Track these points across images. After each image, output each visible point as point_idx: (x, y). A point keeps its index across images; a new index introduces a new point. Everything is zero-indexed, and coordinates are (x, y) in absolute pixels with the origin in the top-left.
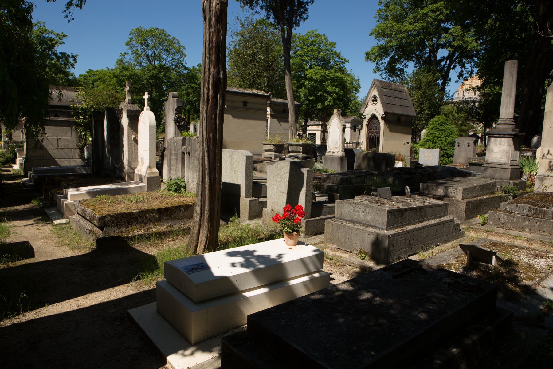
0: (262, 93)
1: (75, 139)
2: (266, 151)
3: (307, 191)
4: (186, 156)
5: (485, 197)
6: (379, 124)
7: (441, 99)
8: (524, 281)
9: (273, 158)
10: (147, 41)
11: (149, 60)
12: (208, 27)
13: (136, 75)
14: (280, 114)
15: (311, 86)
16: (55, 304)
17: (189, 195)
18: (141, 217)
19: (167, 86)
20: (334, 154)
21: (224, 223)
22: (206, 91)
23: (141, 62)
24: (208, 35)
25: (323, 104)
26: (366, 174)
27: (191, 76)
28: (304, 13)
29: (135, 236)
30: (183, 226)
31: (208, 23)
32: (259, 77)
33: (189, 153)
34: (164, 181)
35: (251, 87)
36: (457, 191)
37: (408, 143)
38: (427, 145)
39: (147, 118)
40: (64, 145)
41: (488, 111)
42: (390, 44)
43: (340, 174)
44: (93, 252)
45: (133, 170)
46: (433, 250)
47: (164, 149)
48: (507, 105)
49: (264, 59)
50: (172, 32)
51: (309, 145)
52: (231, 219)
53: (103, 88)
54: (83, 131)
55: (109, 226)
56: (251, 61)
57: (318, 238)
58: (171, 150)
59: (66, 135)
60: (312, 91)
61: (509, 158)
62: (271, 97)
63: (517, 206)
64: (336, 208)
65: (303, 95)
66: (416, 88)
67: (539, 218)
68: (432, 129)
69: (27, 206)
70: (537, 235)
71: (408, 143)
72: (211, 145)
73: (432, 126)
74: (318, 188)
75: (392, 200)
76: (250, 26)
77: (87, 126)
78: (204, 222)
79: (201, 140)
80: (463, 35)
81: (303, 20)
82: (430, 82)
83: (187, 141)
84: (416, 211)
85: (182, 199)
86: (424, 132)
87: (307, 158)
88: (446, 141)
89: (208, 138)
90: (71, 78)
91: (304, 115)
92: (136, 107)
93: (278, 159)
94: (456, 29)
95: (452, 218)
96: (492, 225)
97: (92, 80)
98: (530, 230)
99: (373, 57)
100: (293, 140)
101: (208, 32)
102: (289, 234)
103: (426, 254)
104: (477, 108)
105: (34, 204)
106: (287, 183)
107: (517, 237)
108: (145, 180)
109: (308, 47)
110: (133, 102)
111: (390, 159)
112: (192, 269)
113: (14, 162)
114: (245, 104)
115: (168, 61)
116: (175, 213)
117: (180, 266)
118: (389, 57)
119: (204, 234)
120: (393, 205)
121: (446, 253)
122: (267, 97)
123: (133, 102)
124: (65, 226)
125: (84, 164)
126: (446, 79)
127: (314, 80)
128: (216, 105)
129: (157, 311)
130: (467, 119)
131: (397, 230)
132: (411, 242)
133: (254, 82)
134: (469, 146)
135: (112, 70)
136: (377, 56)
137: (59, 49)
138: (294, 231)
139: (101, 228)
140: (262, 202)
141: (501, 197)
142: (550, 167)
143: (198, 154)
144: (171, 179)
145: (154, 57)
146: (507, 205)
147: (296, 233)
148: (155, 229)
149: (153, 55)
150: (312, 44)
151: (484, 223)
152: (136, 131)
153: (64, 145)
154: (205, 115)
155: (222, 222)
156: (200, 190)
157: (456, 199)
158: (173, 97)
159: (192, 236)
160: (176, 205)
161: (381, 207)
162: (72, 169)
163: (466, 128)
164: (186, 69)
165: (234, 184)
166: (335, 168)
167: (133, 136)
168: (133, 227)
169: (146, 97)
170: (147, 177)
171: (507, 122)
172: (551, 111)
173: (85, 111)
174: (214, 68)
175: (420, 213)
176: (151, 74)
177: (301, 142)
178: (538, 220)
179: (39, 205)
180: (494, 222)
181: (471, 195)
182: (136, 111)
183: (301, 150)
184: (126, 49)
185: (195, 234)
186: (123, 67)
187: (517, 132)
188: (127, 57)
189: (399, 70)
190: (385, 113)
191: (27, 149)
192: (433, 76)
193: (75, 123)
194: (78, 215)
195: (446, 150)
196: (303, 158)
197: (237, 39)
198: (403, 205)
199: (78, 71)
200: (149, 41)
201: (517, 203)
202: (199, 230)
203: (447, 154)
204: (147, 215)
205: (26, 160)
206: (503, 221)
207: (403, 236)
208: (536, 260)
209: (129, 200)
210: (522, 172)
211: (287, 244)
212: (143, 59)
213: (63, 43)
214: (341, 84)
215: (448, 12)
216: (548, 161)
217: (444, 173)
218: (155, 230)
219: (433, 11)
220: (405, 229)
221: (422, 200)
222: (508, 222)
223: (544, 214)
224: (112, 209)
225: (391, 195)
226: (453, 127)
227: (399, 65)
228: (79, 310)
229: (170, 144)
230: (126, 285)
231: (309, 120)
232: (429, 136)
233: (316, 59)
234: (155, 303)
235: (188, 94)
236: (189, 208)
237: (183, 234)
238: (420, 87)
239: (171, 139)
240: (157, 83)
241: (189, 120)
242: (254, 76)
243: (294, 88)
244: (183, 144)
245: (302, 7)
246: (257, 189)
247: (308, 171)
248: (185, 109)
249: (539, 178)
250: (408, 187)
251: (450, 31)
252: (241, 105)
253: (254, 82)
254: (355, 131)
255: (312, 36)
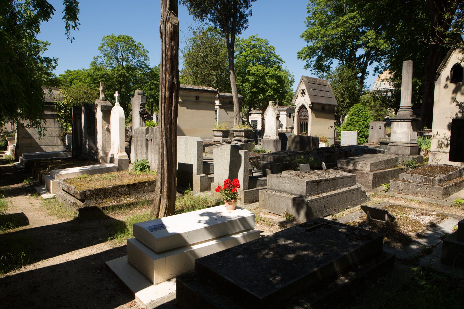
0: (211, 89)
1: (57, 129)
2: (215, 136)
3: (245, 168)
4: (149, 142)
5: (389, 170)
6: (307, 112)
7: (360, 90)
8: (410, 233)
9: (221, 142)
10: (117, 46)
11: (118, 62)
12: (164, 44)
13: (107, 74)
14: (227, 105)
15: (254, 81)
16: (49, 259)
17: (152, 173)
18: (114, 191)
19: (133, 83)
20: (270, 138)
21: (180, 195)
22: (163, 93)
23: (112, 63)
24: (164, 50)
25: (264, 94)
26: (297, 152)
27: (153, 75)
28: (245, 22)
29: (110, 206)
30: (147, 198)
31: (164, 41)
32: (209, 76)
33: (152, 140)
34: (132, 162)
35: (202, 84)
36: (365, 165)
37: (332, 127)
38: (348, 129)
39: (117, 112)
40: (51, 137)
41: (394, 101)
42: (317, 45)
43: (273, 154)
44: (76, 219)
45: (106, 154)
46: (344, 212)
47: (132, 137)
48: (405, 96)
49: (213, 60)
50: (137, 40)
51: (250, 131)
52: (186, 192)
53: (80, 86)
54: (64, 123)
55: (88, 199)
56: (202, 62)
57: (255, 205)
58: (137, 137)
59: (50, 127)
60: (255, 85)
61: (408, 138)
62: (219, 92)
63: (412, 176)
64: (267, 181)
65: (247, 88)
66: (339, 82)
67: (429, 185)
68: (352, 115)
69: (20, 185)
70: (427, 199)
71: (332, 127)
72: (168, 134)
73: (352, 112)
74: (256, 165)
75: (311, 174)
76: (201, 34)
77: (67, 119)
78: (164, 194)
79: (161, 130)
80: (376, 39)
81: (244, 29)
82: (350, 77)
83: (150, 130)
84: (330, 182)
85: (146, 177)
86: (346, 117)
87: (248, 141)
88: (363, 124)
89: (166, 129)
90: (52, 77)
91: (248, 104)
92: (108, 103)
93: (225, 143)
94: (371, 34)
95: (359, 187)
96: (393, 191)
97: (71, 78)
98: (422, 194)
99: (303, 55)
100: (237, 126)
101: (164, 48)
102: (229, 201)
103: (338, 215)
104: (390, 97)
105: (25, 183)
106: (229, 162)
107: (411, 200)
108: (116, 162)
109: (251, 49)
110: (106, 99)
111: (316, 140)
112: (154, 228)
113: (6, 149)
114: (197, 98)
115: (134, 62)
116: (141, 187)
117: (145, 226)
118: (317, 56)
119: (164, 203)
120: (311, 177)
121: (354, 214)
122: (216, 92)
123: (106, 99)
124: (53, 200)
125: (65, 150)
126: (364, 72)
127: (257, 76)
128: (171, 103)
129: (128, 262)
130: (381, 106)
131: (314, 197)
132: (326, 206)
133: (205, 79)
134: (380, 129)
135: (87, 70)
136: (307, 55)
137: (43, 55)
138: (232, 199)
139: (82, 201)
140: (211, 178)
141: (402, 169)
142: (439, 145)
143: (159, 141)
144: (137, 161)
145: (122, 59)
146: (404, 175)
147: (233, 200)
148: (125, 201)
149: (121, 57)
150: (255, 46)
151: (388, 190)
152: (109, 122)
153: (51, 137)
154: (163, 111)
155: (178, 194)
156: (160, 169)
157: (365, 172)
158: (138, 95)
159: (154, 206)
160: (142, 181)
161: (301, 179)
162: (55, 154)
163: (383, 113)
164: (149, 69)
165: (188, 165)
166: (270, 149)
167: (106, 127)
168: (108, 199)
169: (117, 95)
170: (118, 160)
171: (406, 110)
172: (438, 100)
173: (65, 106)
174: (169, 75)
175: (333, 183)
176: (120, 73)
177: (243, 128)
178: (427, 187)
179: (30, 184)
180: (395, 189)
181: (377, 169)
182: (109, 106)
183: (244, 135)
184: (99, 53)
185: (157, 204)
186: (96, 68)
187: (415, 117)
188: (100, 60)
189: (326, 67)
190: (312, 103)
191: (18, 138)
192: (352, 71)
193: (58, 116)
194: (63, 191)
195: (364, 132)
196: (245, 141)
197: (190, 44)
198: (319, 177)
199: (58, 72)
200: (119, 47)
201: (412, 174)
202: (160, 200)
203: (364, 135)
204: (119, 190)
205: (17, 147)
206: (401, 189)
207: (319, 201)
208: (422, 217)
209: (104, 178)
210: (420, 149)
211: (227, 209)
212: (113, 61)
213: (46, 49)
214: (279, 79)
215: (363, 19)
216: (438, 140)
217: (359, 151)
218: (125, 201)
219: (351, 19)
220: (320, 196)
221: (335, 173)
222: (405, 189)
223: (433, 182)
224: (91, 185)
225: (310, 169)
226: (369, 112)
227: (326, 63)
228: (67, 262)
229: (136, 133)
230: (103, 243)
231: (252, 109)
232: (350, 121)
233: (257, 58)
234: (127, 256)
235: (151, 90)
236: (152, 183)
237: (147, 204)
238: (342, 80)
239: (137, 129)
240: (124, 81)
241: (152, 111)
242: (205, 75)
243: (239, 83)
244: (147, 133)
245: (243, 19)
246: (206, 167)
247: (245, 152)
248: (148, 102)
249: (432, 153)
250: (324, 163)
251: (366, 34)
252: (194, 99)
253: (205, 79)
254: (290, 117)
255: (253, 40)
